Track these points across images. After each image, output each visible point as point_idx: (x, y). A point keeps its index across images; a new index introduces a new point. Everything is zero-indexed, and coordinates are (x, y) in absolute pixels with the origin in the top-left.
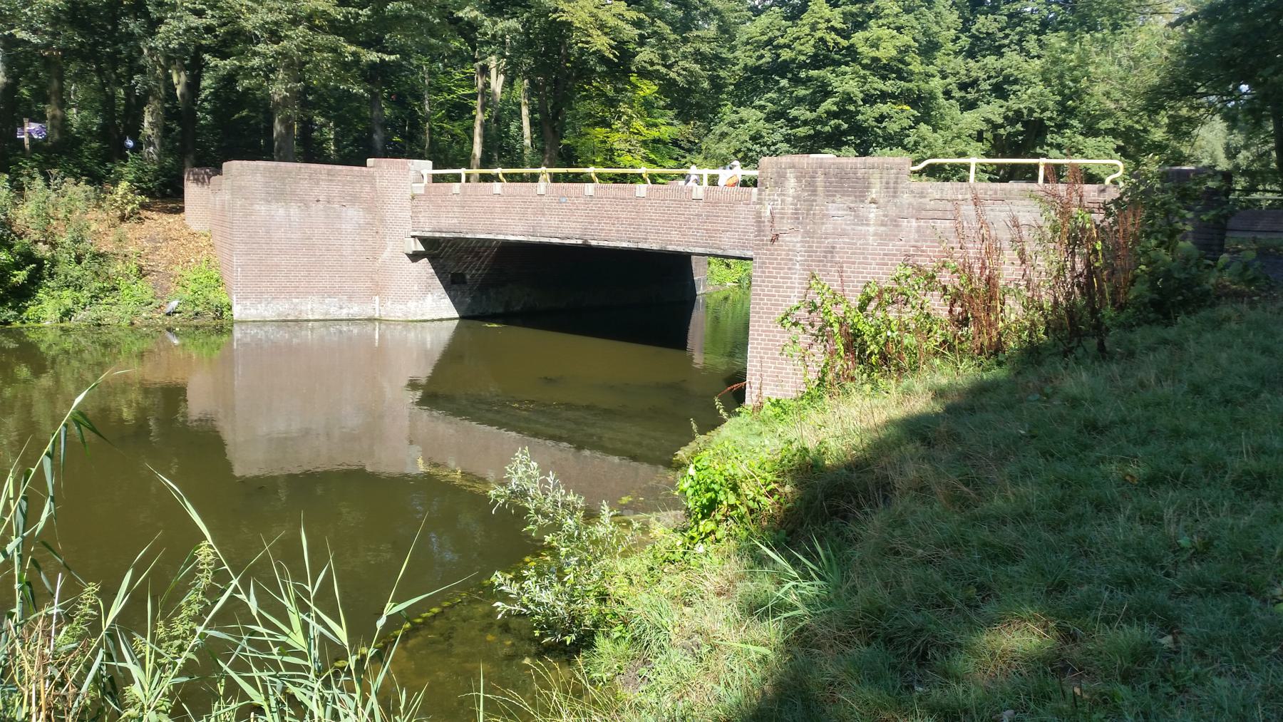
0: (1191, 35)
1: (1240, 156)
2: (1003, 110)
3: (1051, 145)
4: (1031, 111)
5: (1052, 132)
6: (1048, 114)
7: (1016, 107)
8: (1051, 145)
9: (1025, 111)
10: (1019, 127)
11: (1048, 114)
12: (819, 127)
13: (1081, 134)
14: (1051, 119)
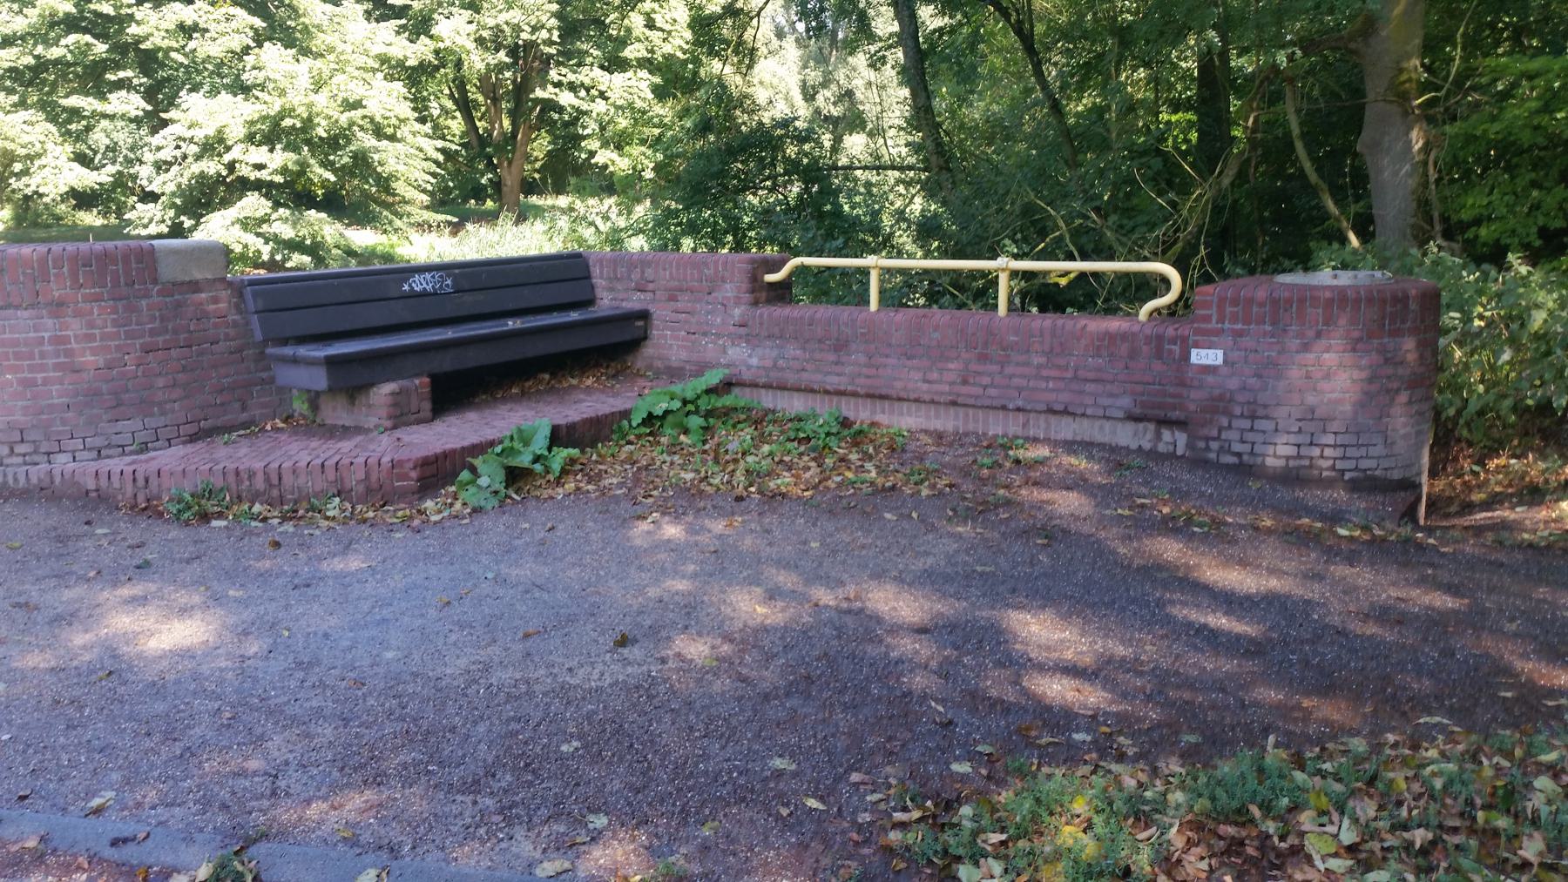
0: (1029, 156)
1: (820, 97)
2: (473, 27)
3: (558, 85)
4: (517, 29)
5: (559, 64)
6: (544, 34)
7: (491, 22)
8: (558, 85)
9: (507, 30)
10: (502, 56)
11: (544, 34)
12: (39, 50)
13: (602, 67)
14: (550, 43)
